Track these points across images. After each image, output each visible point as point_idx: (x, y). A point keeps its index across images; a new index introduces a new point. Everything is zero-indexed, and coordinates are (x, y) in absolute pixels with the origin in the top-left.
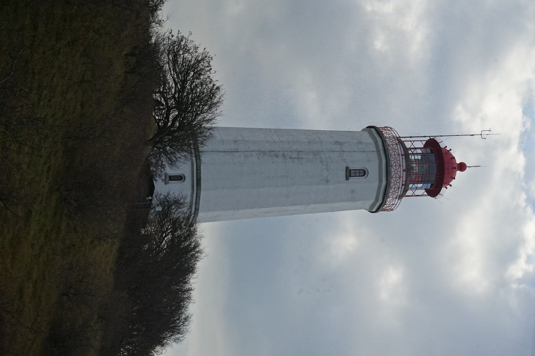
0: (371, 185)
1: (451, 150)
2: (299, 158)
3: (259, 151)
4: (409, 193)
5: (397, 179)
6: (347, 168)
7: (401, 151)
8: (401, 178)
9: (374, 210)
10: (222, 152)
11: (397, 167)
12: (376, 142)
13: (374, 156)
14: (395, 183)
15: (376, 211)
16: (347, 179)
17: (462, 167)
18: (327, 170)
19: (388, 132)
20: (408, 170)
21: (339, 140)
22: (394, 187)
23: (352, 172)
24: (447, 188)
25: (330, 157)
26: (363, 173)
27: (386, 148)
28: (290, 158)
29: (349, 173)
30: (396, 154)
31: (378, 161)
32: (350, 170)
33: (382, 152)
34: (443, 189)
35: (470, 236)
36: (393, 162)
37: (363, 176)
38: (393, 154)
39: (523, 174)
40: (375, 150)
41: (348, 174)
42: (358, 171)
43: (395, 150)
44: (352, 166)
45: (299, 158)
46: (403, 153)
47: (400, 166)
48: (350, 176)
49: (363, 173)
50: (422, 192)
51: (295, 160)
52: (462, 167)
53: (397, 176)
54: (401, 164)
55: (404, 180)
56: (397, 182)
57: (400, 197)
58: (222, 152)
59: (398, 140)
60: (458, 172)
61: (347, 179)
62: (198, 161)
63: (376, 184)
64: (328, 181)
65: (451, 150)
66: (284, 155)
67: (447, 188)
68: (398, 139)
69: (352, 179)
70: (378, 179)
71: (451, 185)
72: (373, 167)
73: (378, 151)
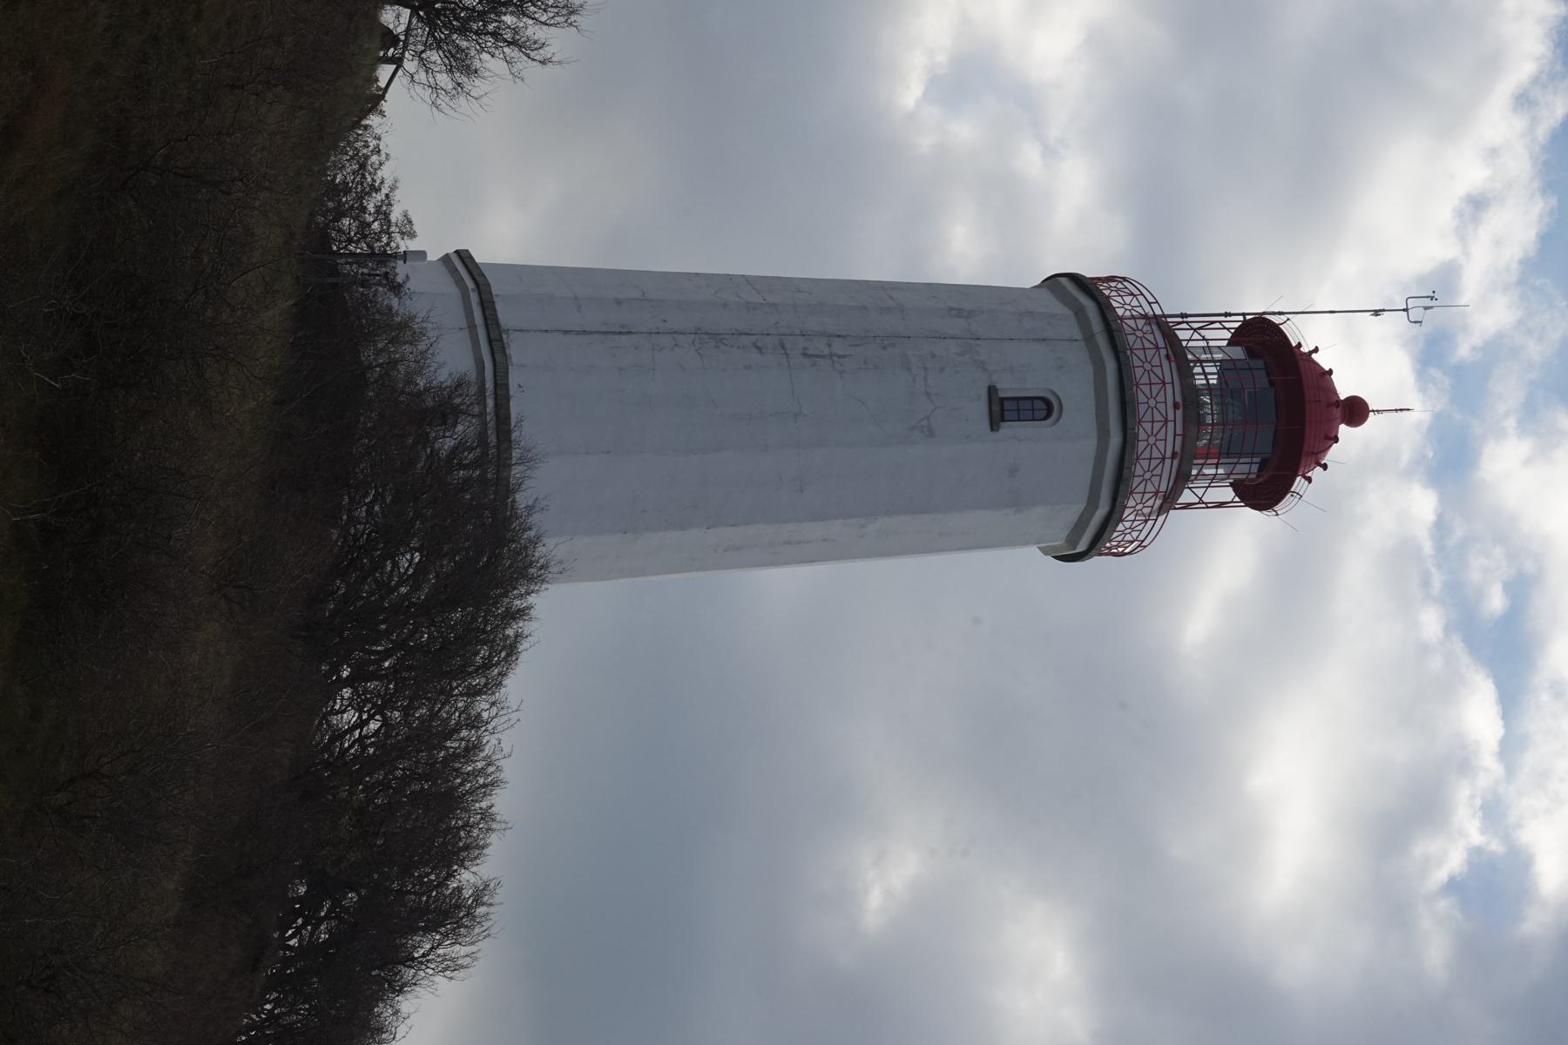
0: (1069, 450)
1: (1316, 350)
2: (831, 355)
3: (697, 332)
4: (1187, 496)
5: (1154, 463)
6: (992, 390)
7: (1172, 393)
8: (1171, 425)
9: (1081, 548)
10: (578, 333)
11: (1155, 389)
12: (1079, 313)
13: (1078, 357)
14: (1148, 475)
15: (1094, 548)
16: (994, 425)
17: (1356, 411)
18: (928, 394)
19: (1128, 299)
20: (1190, 398)
21: (968, 309)
22: (1141, 489)
23: (1007, 405)
24: (1309, 480)
25: (933, 356)
26: (1042, 408)
27: (1114, 326)
28: (805, 355)
29: (1004, 409)
30: (1147, 345)
31: (1090, 369)
32: (1002, 400)
33: (1102, 341)
34: (1299, 483)
35: (1294, 688)
36: (1139, 372)
37: (1045, 418)
38: (1138, 345)
39: (1428, 547)
40: (1078, 334)
41: (996, 408)
42: (1028, 404)
43: (1149, 364)
44: (1009, 387)
45: (831, 355)
46: (1179, 399)
47: (1164, 383)
48: (1003, 420)
49: (1042, 408)
50: (1228, 494)
51: (820, 361)
52: (1356, 411)
53: (1158, 417)
54: (1168, 379)
55: (1179, 431)
56: (1151, 474)
57: (1169, 502)
58: (578, 333)
59: (1158, 325)
60: (1344, 430)
61: (994, 425)
62: (498, 357)
63: (1091, 445)
64: (931, 433)
65: (1316, 350)
66: (783, 347)
67: (1309, 480)
68: (1162, 325)
69: (1007, 429)
70: (1094, 433)
71: (1325, 467)
72: (1075, 383)
73: (1089, 339)
